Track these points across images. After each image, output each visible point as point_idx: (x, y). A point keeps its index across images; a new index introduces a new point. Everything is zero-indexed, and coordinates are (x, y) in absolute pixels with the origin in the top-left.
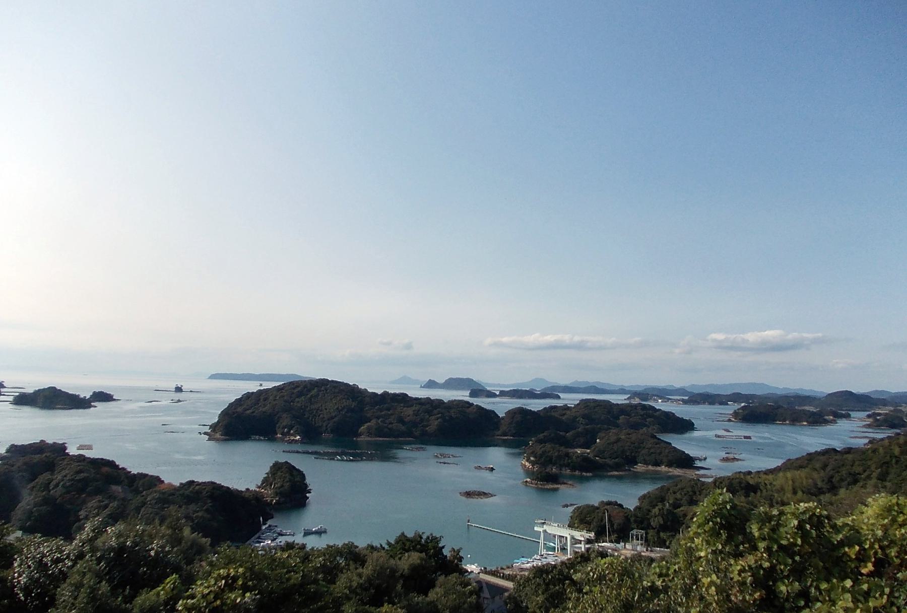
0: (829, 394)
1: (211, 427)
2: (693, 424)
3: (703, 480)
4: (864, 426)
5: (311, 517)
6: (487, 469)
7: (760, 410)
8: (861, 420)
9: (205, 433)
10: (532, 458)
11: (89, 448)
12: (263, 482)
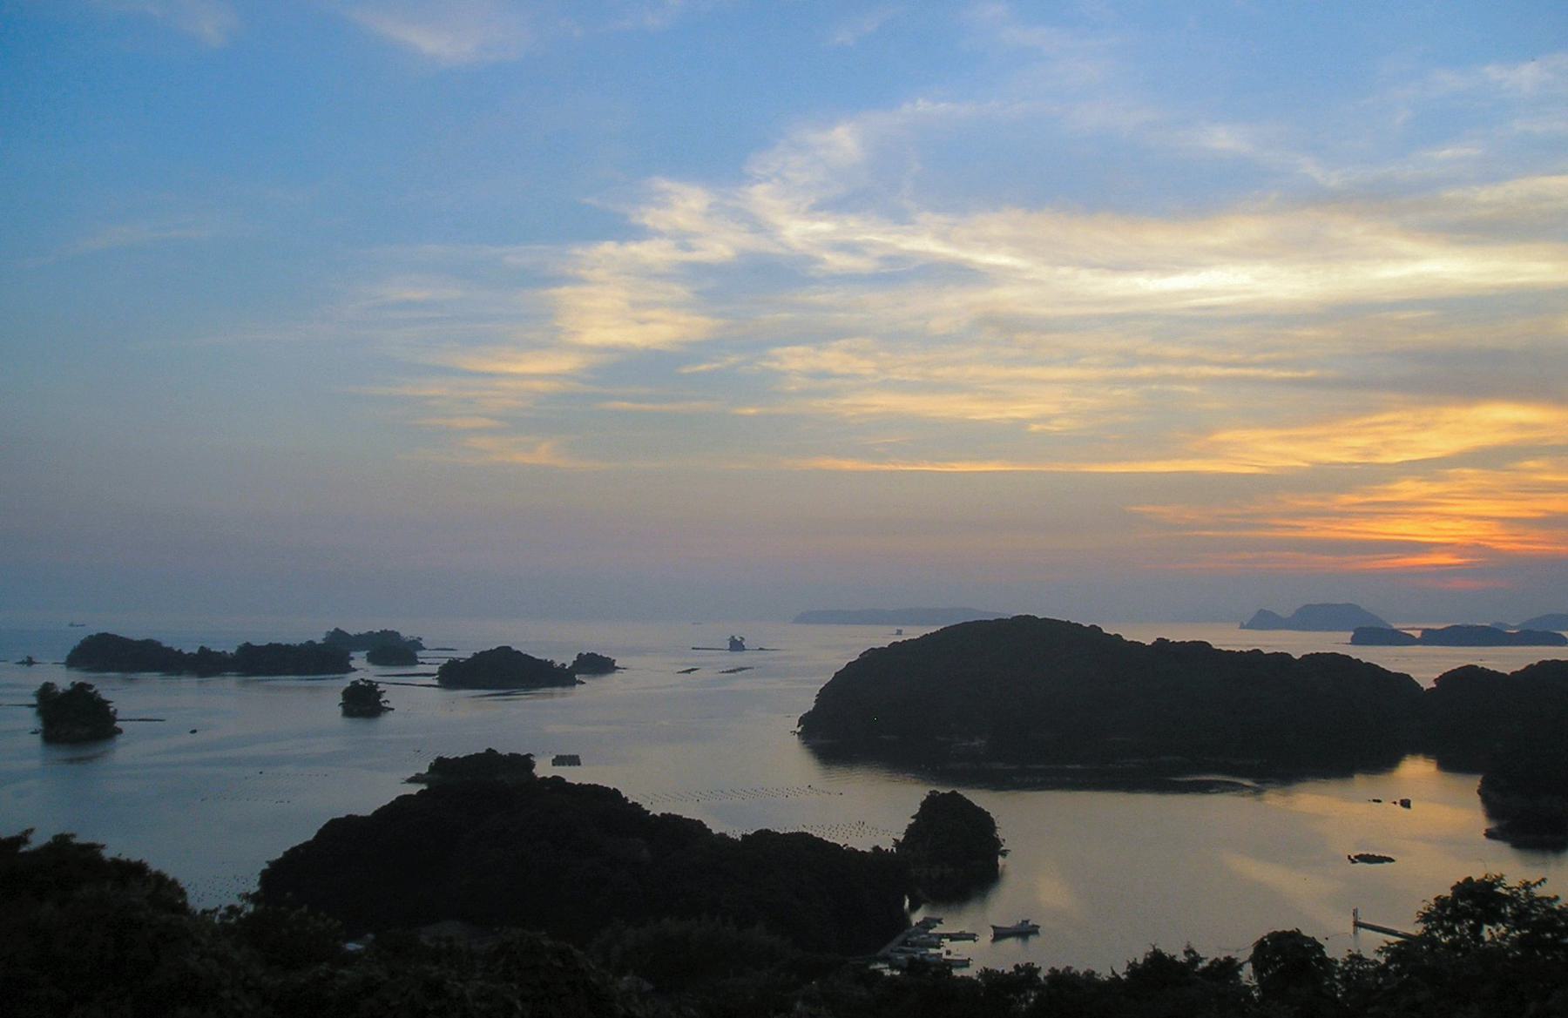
5: (1002, 906)
11: (573, 761)
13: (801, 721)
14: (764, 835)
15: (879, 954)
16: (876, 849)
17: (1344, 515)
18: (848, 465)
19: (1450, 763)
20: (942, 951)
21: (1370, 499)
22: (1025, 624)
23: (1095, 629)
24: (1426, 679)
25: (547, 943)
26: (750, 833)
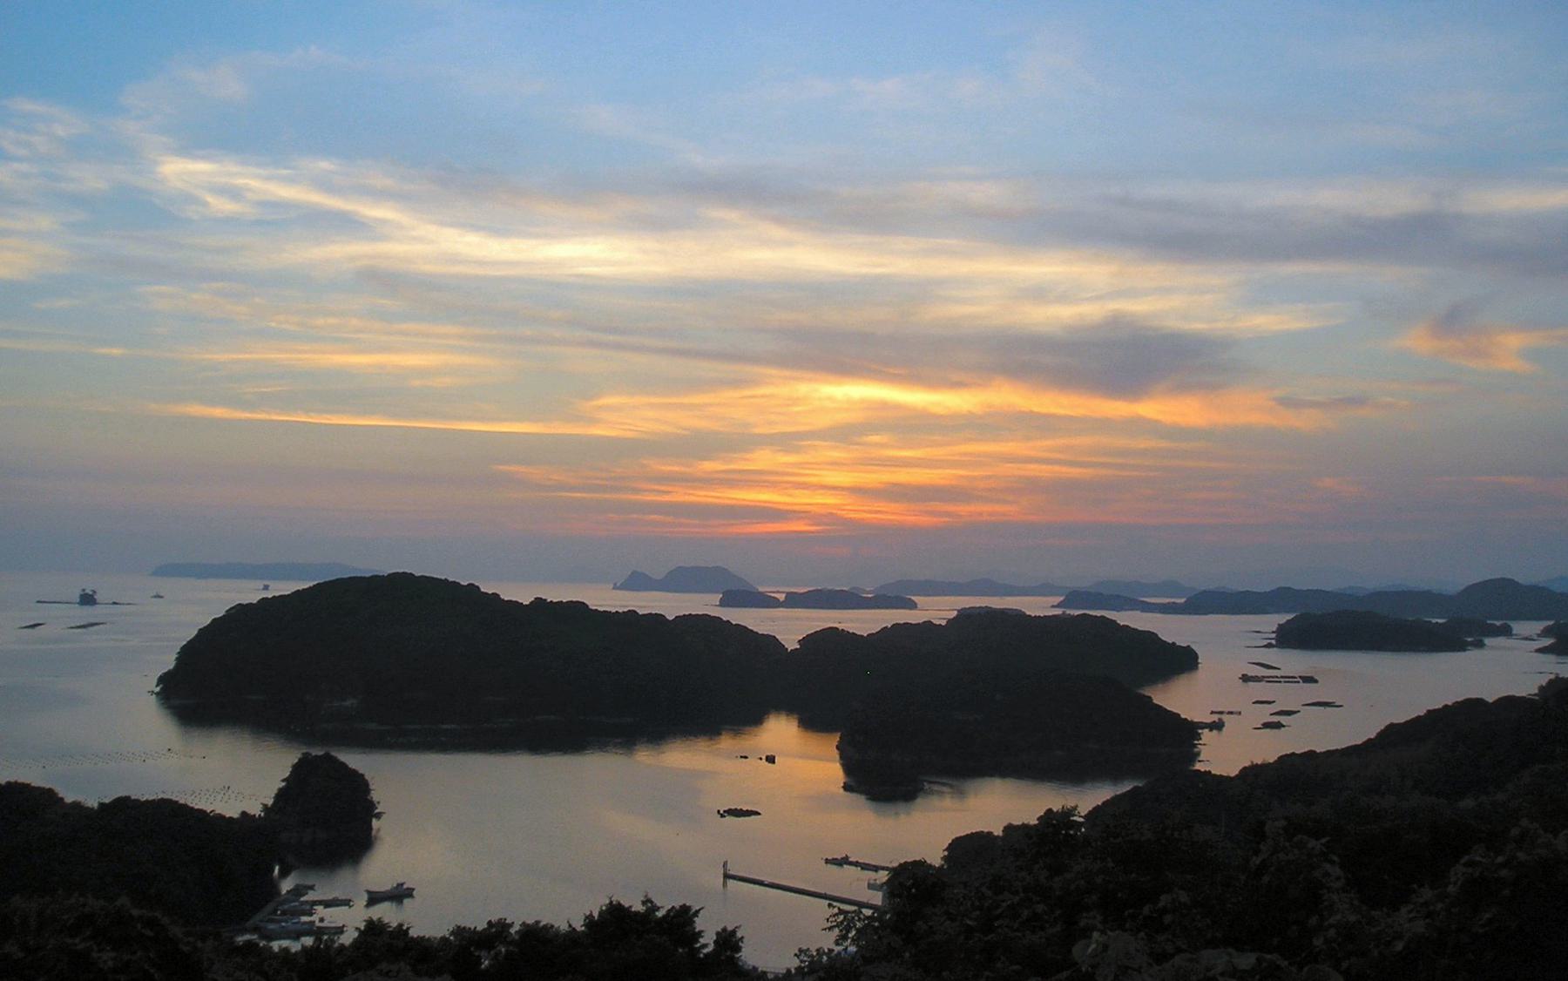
5: (379, 869)
7: (1328, 624)
13: (161, 680)
14: (123, 804)
15: (249, 924)
16: (244, 814)
17: (709, 481)
18: (219, 412)
19: (812, 722)
20: (315, 918)
21: (732, 467)
22: (401, 584)
23: (473, 588)
24: (791, 642)
25: (135, 912)
26: (107, 801)
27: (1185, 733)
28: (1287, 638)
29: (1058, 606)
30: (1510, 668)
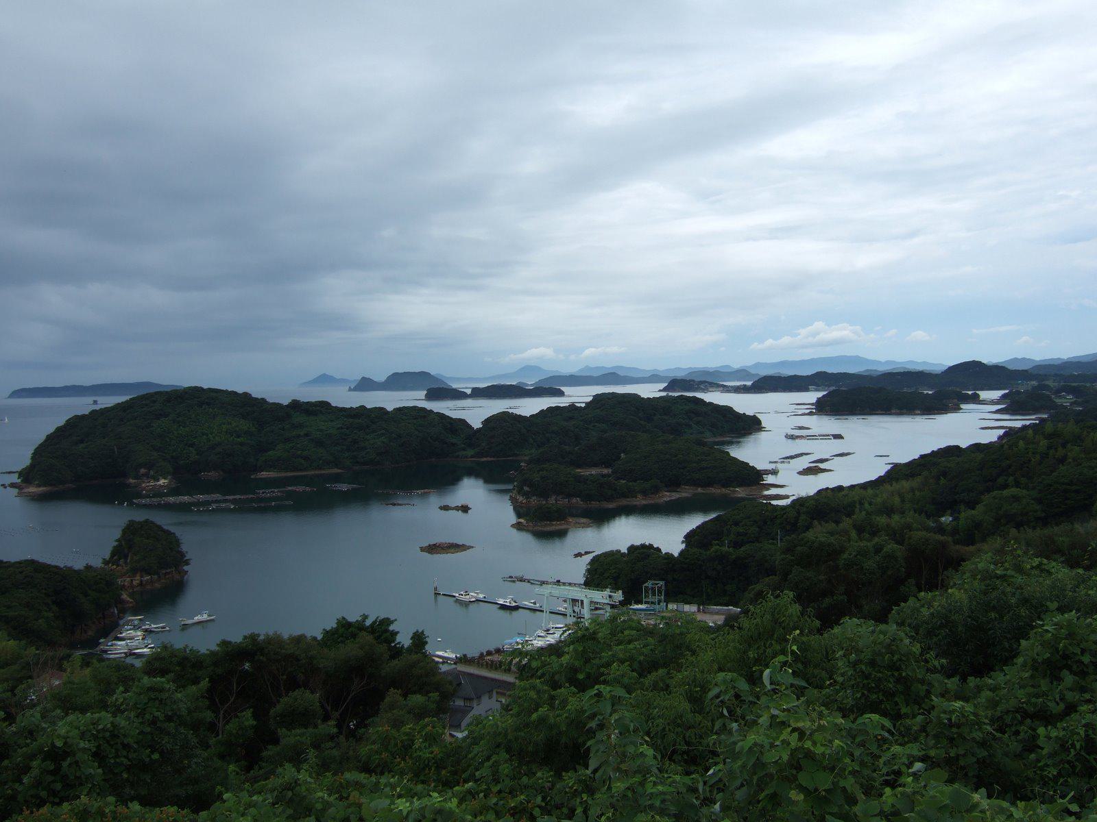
0: (951, 368)
1: (21, 474)
2: (388, 619)
3: (774, 502)
4: (998, 412)
6: (457, 508)
7: (855, 394)
8: (993, 402)
9: (13, 485)
10: (526, 488)
12: (113, 554)
24: (476, 424)
27: (753, 477)
28: (821, 408)
29: (660, 391)
30: (973, 426)
